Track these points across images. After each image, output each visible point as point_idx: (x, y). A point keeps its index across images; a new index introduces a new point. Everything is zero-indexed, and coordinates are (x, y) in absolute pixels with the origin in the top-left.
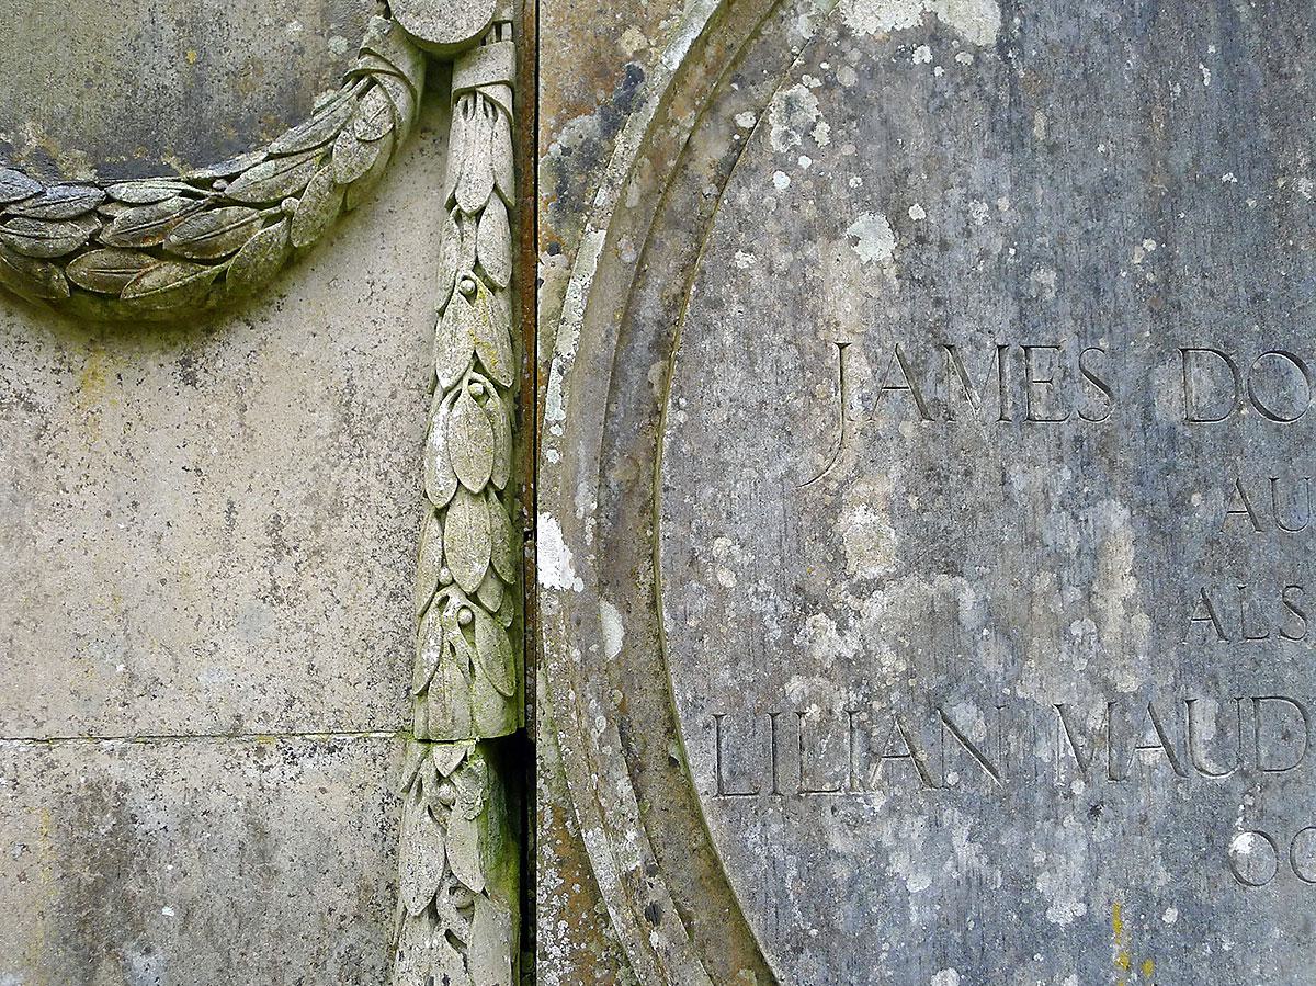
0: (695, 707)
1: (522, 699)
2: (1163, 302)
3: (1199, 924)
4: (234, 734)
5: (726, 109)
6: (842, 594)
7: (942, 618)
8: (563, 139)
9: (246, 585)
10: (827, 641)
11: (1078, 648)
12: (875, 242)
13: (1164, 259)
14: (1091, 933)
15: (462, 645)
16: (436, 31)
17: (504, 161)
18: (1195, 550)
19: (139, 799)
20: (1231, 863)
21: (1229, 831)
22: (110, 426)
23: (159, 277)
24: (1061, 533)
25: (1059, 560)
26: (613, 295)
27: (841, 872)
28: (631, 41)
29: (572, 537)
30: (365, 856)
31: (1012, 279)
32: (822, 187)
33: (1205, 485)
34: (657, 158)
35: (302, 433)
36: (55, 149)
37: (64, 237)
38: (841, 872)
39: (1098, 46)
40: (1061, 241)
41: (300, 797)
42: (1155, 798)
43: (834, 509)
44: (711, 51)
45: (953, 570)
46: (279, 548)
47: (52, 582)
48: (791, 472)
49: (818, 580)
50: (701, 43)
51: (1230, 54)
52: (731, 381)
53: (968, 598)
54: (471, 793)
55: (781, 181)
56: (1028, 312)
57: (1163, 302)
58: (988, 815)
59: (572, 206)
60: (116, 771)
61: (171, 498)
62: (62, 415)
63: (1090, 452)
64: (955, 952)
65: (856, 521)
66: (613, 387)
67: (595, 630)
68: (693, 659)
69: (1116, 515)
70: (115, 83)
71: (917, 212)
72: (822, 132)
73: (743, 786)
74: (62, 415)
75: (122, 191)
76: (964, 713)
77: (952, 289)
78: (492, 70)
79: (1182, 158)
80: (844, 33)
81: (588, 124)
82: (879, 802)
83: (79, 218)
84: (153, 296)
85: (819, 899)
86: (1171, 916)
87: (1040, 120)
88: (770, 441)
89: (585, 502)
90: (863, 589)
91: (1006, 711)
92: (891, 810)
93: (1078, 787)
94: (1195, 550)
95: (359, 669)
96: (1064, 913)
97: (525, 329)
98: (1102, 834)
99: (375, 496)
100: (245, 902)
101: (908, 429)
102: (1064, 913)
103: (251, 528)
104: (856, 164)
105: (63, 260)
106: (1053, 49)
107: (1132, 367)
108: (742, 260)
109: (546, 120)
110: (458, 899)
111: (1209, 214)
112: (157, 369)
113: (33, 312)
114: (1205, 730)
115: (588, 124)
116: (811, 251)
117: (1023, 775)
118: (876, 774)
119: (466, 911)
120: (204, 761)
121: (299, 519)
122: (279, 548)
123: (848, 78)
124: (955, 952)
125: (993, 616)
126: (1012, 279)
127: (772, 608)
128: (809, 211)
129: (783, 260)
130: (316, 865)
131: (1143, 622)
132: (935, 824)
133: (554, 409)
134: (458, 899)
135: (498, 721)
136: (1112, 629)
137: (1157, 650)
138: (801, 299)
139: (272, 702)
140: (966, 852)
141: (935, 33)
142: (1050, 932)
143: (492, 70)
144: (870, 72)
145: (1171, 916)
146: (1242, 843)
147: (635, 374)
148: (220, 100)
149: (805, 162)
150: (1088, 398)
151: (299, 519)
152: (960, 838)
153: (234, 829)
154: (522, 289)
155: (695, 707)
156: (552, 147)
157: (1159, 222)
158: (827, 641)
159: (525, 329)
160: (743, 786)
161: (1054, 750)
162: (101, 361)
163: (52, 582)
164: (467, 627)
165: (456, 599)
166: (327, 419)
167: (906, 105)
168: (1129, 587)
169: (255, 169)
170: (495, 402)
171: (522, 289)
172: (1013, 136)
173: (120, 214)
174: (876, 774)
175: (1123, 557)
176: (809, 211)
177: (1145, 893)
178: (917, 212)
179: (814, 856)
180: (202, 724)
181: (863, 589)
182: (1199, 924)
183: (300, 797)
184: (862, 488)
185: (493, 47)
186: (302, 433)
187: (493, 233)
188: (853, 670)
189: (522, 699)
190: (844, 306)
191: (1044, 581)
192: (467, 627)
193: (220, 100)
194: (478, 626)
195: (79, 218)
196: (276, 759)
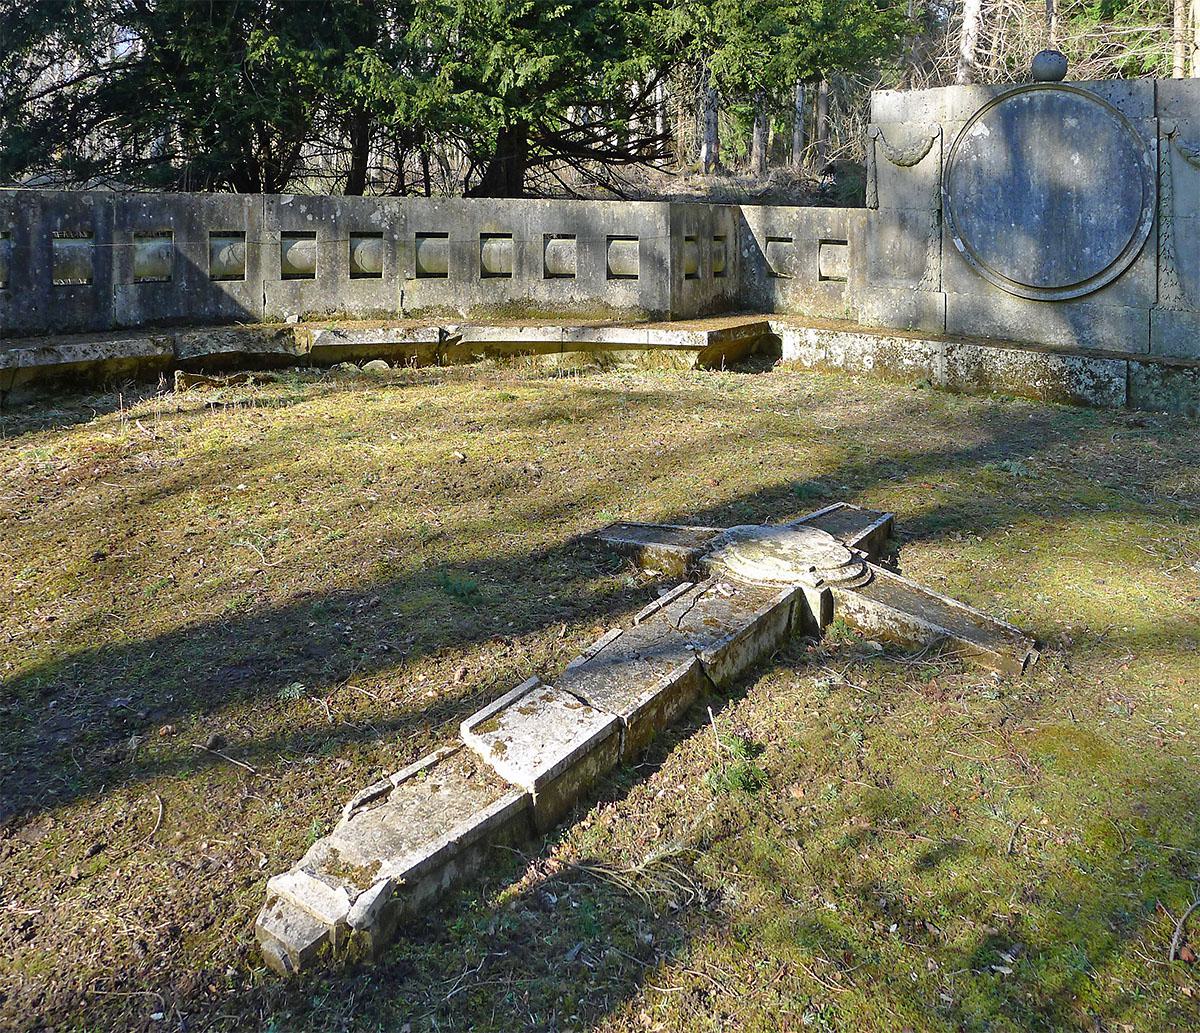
29: (944, 188)
54: (936, 214)
69: (1000, 188)
161: (992, 213)
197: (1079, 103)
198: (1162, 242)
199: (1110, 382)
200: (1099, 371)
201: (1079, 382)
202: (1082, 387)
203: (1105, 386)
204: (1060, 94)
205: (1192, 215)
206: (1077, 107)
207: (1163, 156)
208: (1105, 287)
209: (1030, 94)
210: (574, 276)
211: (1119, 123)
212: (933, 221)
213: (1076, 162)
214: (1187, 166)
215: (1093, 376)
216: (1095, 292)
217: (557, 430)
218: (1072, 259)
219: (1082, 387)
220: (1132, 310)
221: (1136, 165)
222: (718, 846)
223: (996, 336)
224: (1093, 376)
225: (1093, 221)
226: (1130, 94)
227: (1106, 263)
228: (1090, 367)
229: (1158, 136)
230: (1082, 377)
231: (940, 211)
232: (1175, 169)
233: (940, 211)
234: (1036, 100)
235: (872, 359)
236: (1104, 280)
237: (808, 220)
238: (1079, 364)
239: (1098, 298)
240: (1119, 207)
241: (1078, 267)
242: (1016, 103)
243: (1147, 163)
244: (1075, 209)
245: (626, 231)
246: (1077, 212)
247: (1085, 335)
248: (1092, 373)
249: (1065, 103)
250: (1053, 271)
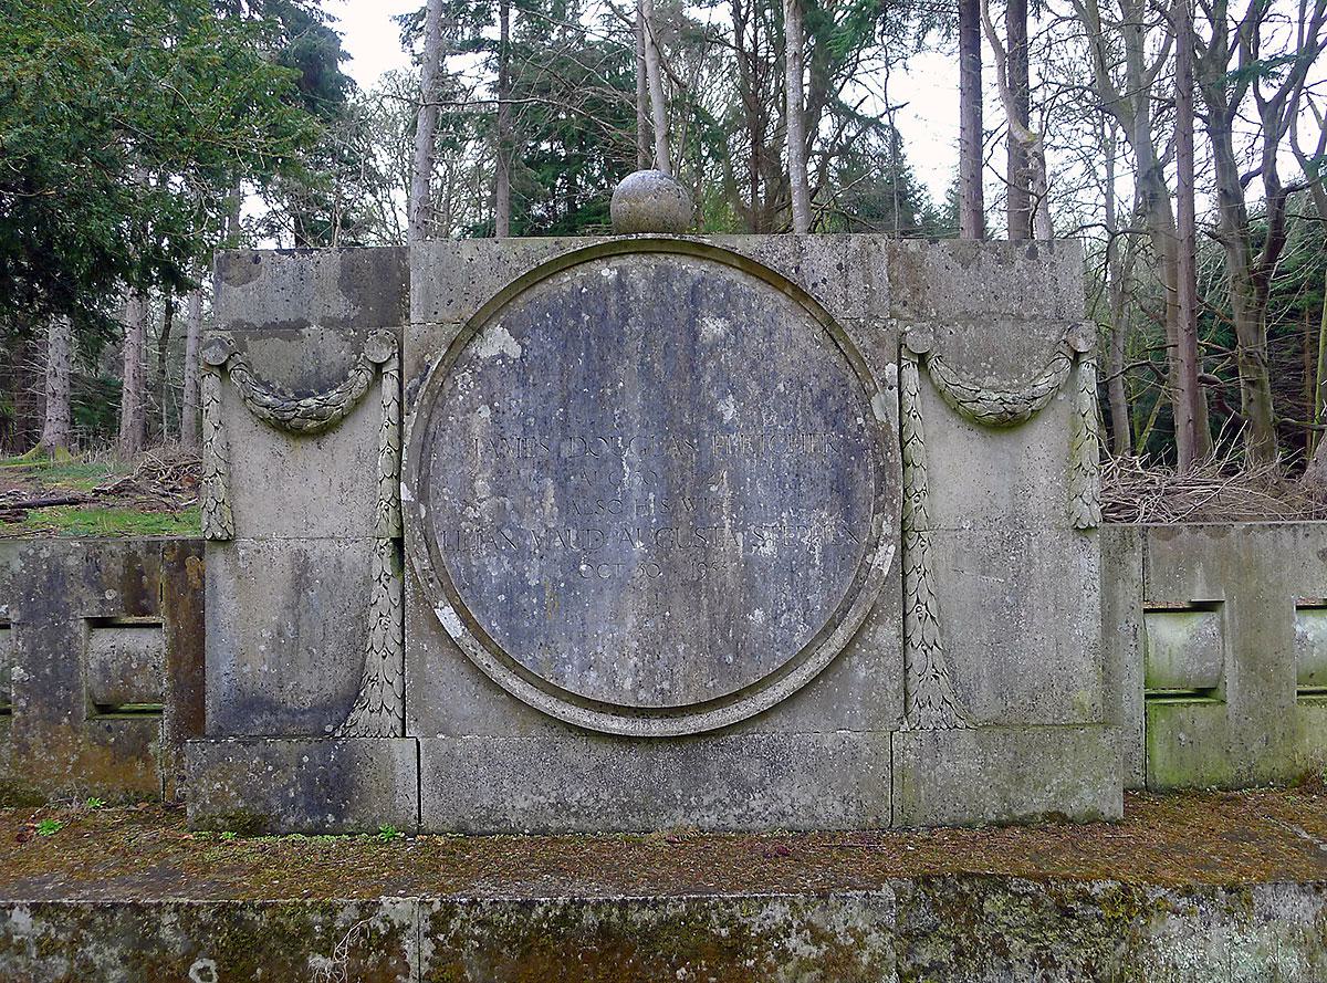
0: (438, 529)
1: (401, 528)
2: (565, 425)
3: (570, 587)
5: (452, 375)
8: (410, 385)
9: (334, 500)
10: (471, 513)
11: (538, 516)
12: (486, 413)
13: (565, 414)
14: (540, 588)
15: (386, 514)
16: (377, 360)
17: (396, 391)
18: (572, 491)
19: (310, 553)
20: (580, 572)
21: (580, 564)
22: (300, 460)
23: (311, 424)
24: (534, 487)
25: (533, 494)
26: (421, 427)
27: (475, 570)
28: (428, 358)
30: (365, 569)
31: (522, 421)
32: (472, 399)
33: (575, 474)
34: (432, 391)
35: (348, 461)
36: (284, 388)
37: (288, 415)
39: (549, 357)
40: (536, 409)
41: (348, 553)
42: (558, 555)
43: (474, 481)
44: (446, 362)
45: (504, 496)
46: (343, 491)
47: (287, 499)
48: (463, 472)
49: (469, 499)
50: (443, 360)
51: (588, 356)
52: (447, 449)
53: (508, 503)
54: (388, 551)
55: (461, 398)
56: (526, 430)
57: (565, 425)
58: (513, 557)
59: (411, 403)
60: (304, 546)
63: (542, 466)
64: (504, 591)
66: (423, 449)
68: (438, 517)
69: (549, 482)
70: (298, 370)
71: (496, 404)
73: (451, 548)
75: (302, 402)
76: (507, 532)
77: (505, 424)
78: (392, 368)
79: (572, 386)
80: (478, 357)
81: (416, 380)
83: (293, 410)
84: (309, 429)
85: (469, 576)
86: (562, 585)
87: (531, 378)
88: (457, 464)
90: (480, 501)
91: (519, 532)
92: (487, 555)
93: (537, 551)
94: (572, 491)
96: (533, 583)
98: (543, 563)
99: (366, 477)
100: (336, 579)
101: (493, 460)
102: (533, 583)
103: (336, 485)
104: (480, 393)
105: (289, 421)
106: (536, 358)
107: (555, 443)
108: (451, 419)
109: (405, 380)
110: (387, 577)
111: (580, 400)
112: (311, 445)
113: (281, 432)
114: (573, 538)
115: (416, 380)
117: (522, 548)
121: (347, 483)
122: (343, 491)
123: (479, 370)
124: (504, 591)
126: (522, 421)
127: (458, 506)
128: (468, 405)
129: (461, 418)
130: (353, 571)
132: (499, 559)
134: (387, 577)
136: (547, 511)
137: (560, 516)
138: (465, 428)
139: (342, 530)
140: (507, 566)
141: (503, 356)
143: (392, 368)
144: (485, 368)
145: (562, 585)
146: (583, 567)
147: (428, 446)
148: (324, 373)
149: (467, 392)
150: (543, 451)
151: (347, 483)
152: (505, 563)
155: (438, 529)
156: (407, 388)
157: (564, 404)
158: (471, 513)
160: (451, 548)
161: (532, 541)
162: (298, 444)
163: (287, 499)
164: (387, 510)
165: (384, 503)
167: (494, 374)
169: (333, 395)
172: (524, 383)
175: (551, 492)
176: (468, 405)
177: (556, 579)
178: (496, 404)
179: (468, 566)
180: (325, 535)
181: (480, 501)
182: (570, 587)
183: (348, 553)
184: (480, 475)
185: (393, 360)
186: (348, 461)
187: (394, 407)
188: (478, 521)
189: (401, 528)
191: (529, 499)
192: (387, 510)
193: (324, 373)
194: (1269, 108)
195: (293, 410)
196: (342, 544)
198: (911, 588)
205: (967, 524)
207: (910, 401)
208: (797, 694)
210: (1299, 608)
212: (383, 564)
213: (728, 417)
215: (817, 937)
222: (683, 316)
225: (768, 549)
227: (801, 641)
230: (793, 942)
231: (398, 543)
233: (398, 543)
236: (794, 681)
240: (824, 514)
241: (737, 655)
245: (643, 683)
246: (734, 529)
247: (753, 804)
250: (680, 669)
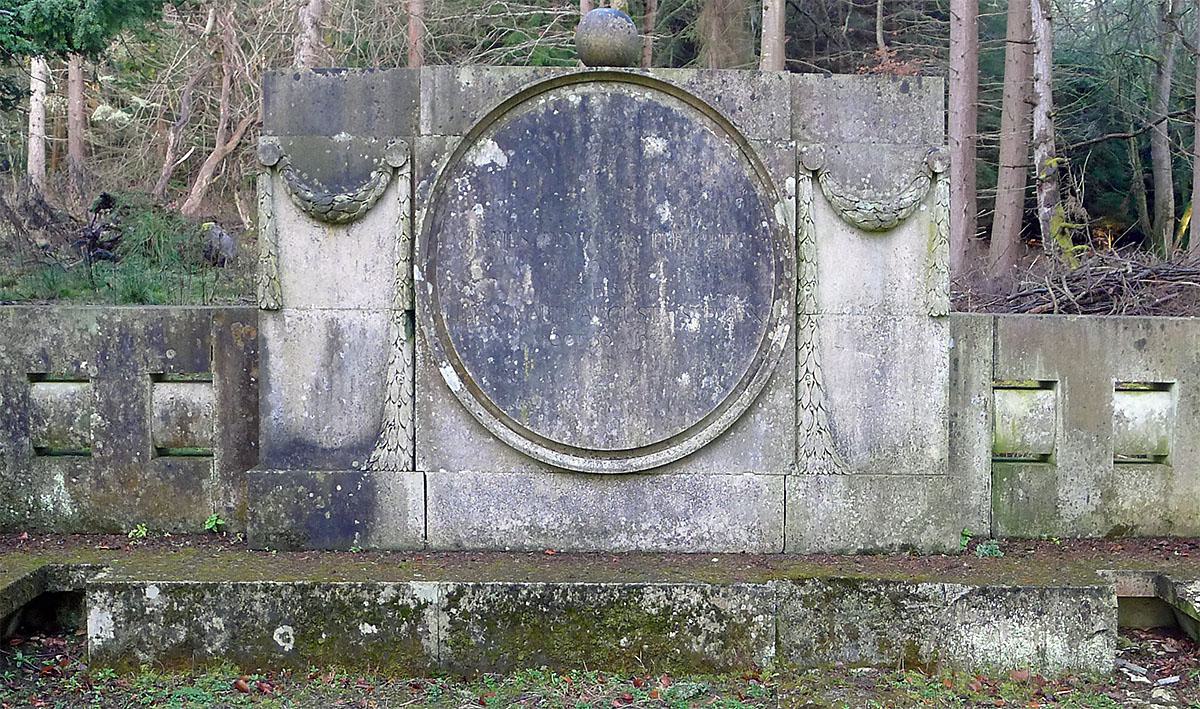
1: (412, 303)
4: (358, 309)
6: (470, 282)
7: (490, 287)
9: (360, 278)
27: (470, 337)
29: (421, 270)
38: (470, 337)
43: (470, 265)
55: (461, 198)
60: (336, 316)
61: (345, 260)
62: (324, 243)
63: (521, 254)
65: (474, 267)
67: (426, 289)
72: (469, 188)
74: (324, 243)
82: (478, 324)
89: (424, 264)
95: (382, 296)
96: (515, 348)
97: (412, 226)
102: (515, 348)
112: (342, 232)
114: (545, 312)
116: (466, 212)
118: (477, 317)
119: (402, 344)
120: (351, 314)
125: (501, 287)
131: (532, 289)
133: (417, 245)
135: (465, 525)
138: (464, 222)
142: (512, 352)
145: (537, 350)
153: (359, 327)
154: (412, 217)
158: (467, 290)
159: (412, 226)
161: (515, 315)
163: (323, 277)
166: (375, 243)
168: (530, 282)
170: (408, 241)
171: (412, 217)
173: (337, 204)
174: (477, 317)
175: (529, 275)
187: (406, 206)
188: (473, 298)
190: (472, 222)
196: (366, 314)
197: (668, 109)
199: (750, 622)
200: (729, 606)
201: (696, 630)
202: (701, 638)
203: (743, 630)
204: (634, 93)
206: (665, 117)
209: (580, 89)
211: (735, 148)
214: (839, 225)
216: (697, 453)
217: (437, 109)
218: (659, 396)
219: (701, 638)
220: (755, 478)
221: (765, 224)
223: (523, 545)
224: (720, 617)
226: (753, 97)
228: (713, 600)
229: (798, 174)
231: (411, 314)
232: (283, 225)
233: (411, 314)
234: (594, 101)
235: (290, 630)
237: (123, 336)
238: (695, 598)
239: (700, 466)
242: (558, 104)
243: (780, 220)
244: (662, 303)
247: (679, 531)
248: (718, 611)
249: (647, 107)
